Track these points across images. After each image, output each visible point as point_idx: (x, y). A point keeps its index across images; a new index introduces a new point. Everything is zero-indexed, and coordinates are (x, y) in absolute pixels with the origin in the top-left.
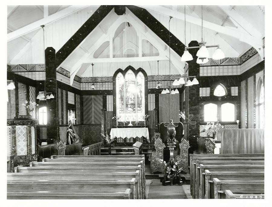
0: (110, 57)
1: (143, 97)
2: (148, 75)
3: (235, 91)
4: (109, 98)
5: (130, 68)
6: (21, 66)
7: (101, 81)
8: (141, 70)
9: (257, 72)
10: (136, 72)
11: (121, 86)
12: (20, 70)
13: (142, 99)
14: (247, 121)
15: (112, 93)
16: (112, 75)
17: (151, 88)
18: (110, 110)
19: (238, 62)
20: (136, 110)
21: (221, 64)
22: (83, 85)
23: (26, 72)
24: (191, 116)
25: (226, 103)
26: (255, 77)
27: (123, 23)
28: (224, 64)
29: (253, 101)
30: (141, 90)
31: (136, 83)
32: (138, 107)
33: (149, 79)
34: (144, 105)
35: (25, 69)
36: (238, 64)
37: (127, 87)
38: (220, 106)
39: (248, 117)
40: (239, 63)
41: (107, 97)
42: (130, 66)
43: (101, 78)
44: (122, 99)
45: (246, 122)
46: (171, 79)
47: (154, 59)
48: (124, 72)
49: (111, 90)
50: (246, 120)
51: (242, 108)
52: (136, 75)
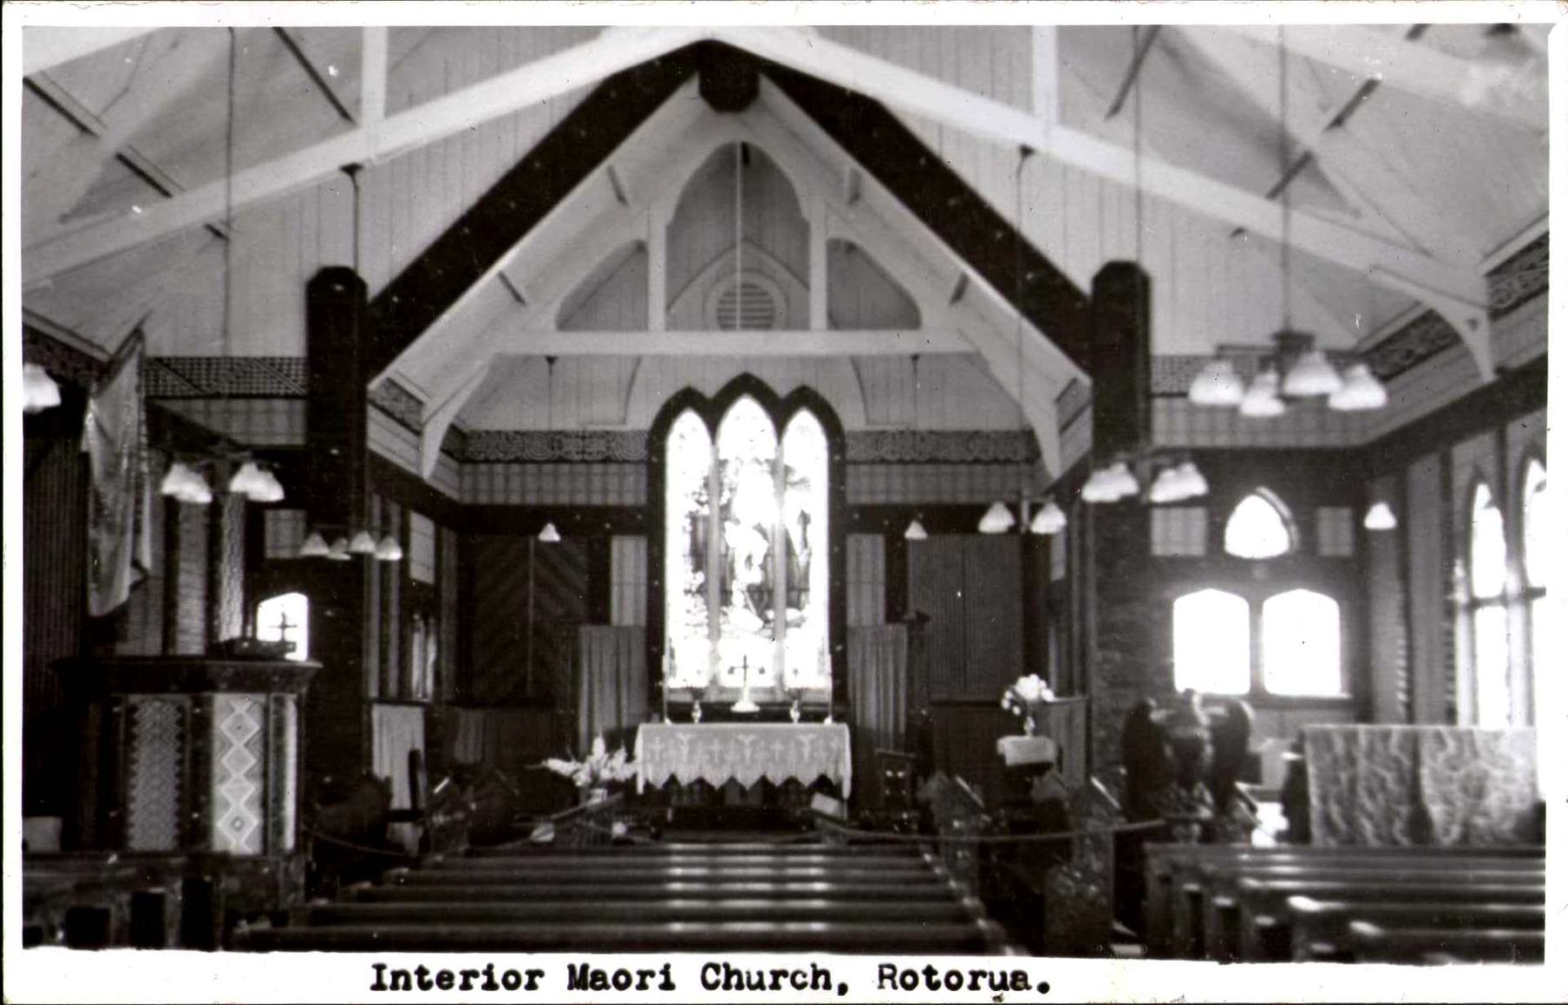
0: (651, 326)
1: (814, 552)
4: (626, 554)
5: (746, 385)
7: (583, 452)
9: (1460, 436)
10: (780, 411)
12: (152, 388)
14: (1410, 691)
17: (865, 499)
18: (628, 620)
22: (491, 474)
23: (197, 397)
24: (1106, 660)
25: (1204, 587)
26: (1446, 463)
29: (1437, 585)
39: (1410, 670)
41: (616, 544)
43: (584, 438)
44: (699, 556)
45: (1402, 697)
46: (976, 453)
47: (903, 342)
49: (639, 509)
50: (1402, 684)
51: (1376, 619)
52: (780, 426)
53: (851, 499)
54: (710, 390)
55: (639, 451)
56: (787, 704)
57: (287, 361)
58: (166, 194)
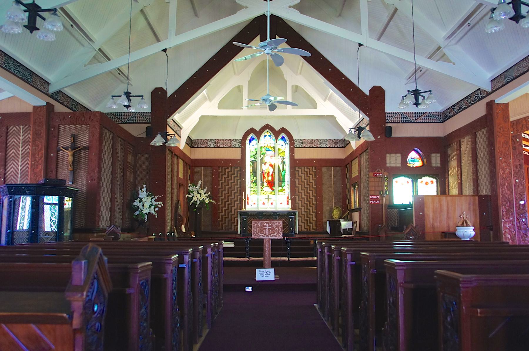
2: (294, 138)
3: (436, 160)
5: (267, 127)
6: (113, 115)
7: (224, 145)
8: (283, 130)
10: (276, 133)
11: (253, 154)
13: (285, 175)
15: (241, 163)
16: (241, 137)
19: (439, 118)
20: (277, 191)
21: (416, 120)
27: (264, 61)
28: (420, 120)
30: (284, 160)
31: (276, 149)
32: (279, 186)
33: (297, 144)
34: (289, 183)
35: (119, 119)
36: (439, 121)
37: (262, 156)
38: (416, 181)
40: (441, 119)
42: (267, 125)
43: (224, 141)
46: (329, 145)
48: (258, 134)
53: (296, 157)
54: (258, 129)
55: (238, 144)
56: (179, 268)
57: (145, 113)
58: (109, 60)
